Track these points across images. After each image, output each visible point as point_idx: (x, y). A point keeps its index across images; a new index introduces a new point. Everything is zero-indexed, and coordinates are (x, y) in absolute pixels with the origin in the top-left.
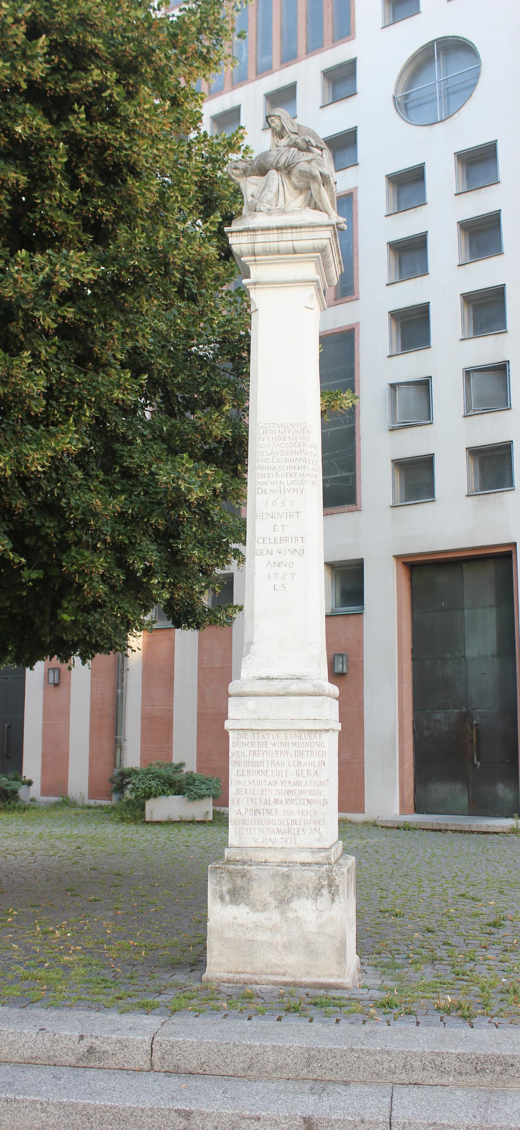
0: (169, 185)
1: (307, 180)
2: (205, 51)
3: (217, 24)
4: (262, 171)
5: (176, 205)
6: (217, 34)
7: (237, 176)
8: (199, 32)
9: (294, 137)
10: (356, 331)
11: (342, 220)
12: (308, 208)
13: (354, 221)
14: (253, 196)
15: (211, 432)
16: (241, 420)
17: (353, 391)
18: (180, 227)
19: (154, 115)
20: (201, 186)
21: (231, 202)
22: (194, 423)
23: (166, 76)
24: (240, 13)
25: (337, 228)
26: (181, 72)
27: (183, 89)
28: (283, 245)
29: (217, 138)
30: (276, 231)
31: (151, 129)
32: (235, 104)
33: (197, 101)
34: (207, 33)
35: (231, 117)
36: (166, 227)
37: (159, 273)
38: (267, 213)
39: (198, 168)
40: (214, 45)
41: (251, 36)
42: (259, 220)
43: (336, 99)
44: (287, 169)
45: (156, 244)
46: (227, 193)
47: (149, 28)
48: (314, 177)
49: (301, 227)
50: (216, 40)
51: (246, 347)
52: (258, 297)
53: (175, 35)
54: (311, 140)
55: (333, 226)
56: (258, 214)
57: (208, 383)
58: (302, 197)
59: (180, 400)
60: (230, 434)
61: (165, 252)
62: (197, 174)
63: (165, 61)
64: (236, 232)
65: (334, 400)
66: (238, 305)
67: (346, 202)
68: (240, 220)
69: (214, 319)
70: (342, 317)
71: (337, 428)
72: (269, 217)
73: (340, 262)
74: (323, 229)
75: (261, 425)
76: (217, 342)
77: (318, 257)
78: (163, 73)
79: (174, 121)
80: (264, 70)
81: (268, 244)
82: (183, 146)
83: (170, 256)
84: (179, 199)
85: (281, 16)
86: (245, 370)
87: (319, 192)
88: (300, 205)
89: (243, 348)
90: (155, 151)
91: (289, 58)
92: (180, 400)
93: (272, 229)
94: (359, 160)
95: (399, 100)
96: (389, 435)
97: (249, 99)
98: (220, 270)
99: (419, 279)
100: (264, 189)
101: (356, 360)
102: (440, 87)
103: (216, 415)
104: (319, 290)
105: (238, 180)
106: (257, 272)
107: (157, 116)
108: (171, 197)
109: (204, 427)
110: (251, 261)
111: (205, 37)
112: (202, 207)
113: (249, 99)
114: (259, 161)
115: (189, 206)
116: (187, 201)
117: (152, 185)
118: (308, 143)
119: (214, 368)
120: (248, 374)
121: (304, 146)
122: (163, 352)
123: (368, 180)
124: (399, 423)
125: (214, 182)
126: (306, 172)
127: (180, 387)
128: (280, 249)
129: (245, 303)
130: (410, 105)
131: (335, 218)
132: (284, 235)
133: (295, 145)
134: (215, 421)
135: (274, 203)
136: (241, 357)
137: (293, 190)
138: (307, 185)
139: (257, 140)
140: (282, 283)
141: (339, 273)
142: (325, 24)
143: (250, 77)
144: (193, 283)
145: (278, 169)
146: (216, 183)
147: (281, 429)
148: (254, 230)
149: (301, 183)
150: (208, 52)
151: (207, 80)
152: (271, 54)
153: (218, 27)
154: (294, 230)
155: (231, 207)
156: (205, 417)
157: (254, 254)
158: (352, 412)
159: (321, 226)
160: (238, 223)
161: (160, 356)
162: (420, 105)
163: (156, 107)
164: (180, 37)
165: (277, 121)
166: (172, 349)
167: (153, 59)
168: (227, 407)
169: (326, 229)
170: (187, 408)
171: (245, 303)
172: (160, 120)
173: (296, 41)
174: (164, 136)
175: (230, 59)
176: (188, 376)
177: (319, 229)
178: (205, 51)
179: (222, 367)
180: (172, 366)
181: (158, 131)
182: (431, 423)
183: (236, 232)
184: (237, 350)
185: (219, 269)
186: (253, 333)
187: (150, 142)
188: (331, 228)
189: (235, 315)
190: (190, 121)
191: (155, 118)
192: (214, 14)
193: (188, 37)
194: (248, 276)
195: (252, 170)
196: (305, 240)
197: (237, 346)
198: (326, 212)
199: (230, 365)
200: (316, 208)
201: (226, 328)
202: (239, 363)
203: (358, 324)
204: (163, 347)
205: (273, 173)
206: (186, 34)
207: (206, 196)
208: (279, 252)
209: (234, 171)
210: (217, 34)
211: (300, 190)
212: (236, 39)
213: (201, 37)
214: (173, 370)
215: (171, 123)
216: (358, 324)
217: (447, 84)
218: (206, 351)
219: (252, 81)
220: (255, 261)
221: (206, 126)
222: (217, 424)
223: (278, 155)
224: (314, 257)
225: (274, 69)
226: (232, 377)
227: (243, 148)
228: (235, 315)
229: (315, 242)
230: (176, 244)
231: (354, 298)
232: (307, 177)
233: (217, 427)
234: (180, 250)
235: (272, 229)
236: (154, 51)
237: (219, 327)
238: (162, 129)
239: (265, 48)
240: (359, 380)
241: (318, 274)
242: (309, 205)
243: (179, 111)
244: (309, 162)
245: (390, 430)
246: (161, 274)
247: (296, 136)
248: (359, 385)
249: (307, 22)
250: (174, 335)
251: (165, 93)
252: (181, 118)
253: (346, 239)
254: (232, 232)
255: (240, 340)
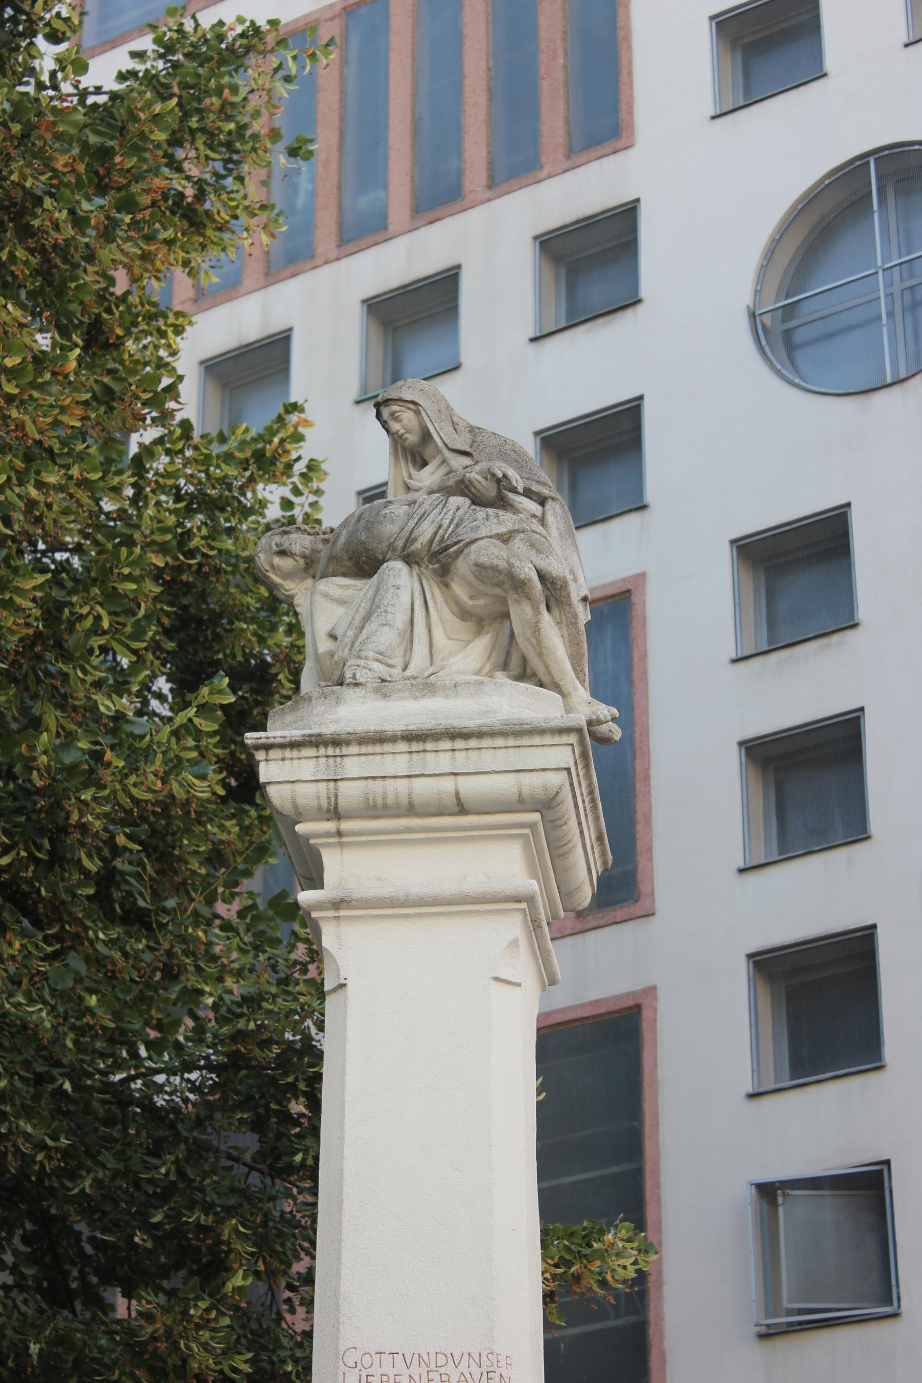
0: (76, 580)
1: (498, 591)
2: (190, 192)
3: (229, 118)
4: (363, 563)
5: (97, 642)
6: (229, 145)
7: (286, 576)
8: (175, 141)
9: (459, 462)
10: (646, 1014)
11: (604, 711)
12: (501, 677)
13: (636, 675)
14: (333, 637)
15: (184, 1361)
16: (280, 1318)
17: (640, 1225)
18: (106, 705)
19: (33, 385)
20: (172, 584)
21: (261, 626)
22: (131, 1332)
23: (76, 266)
24: (292, 87)
25: (592, 738)
26: (119, 256)
27: (123, 298)
28: (424, 788)
29: (223, 439)
30: (402, 746)
31: (21, 426)
32: (276, 326)
33: (162, 334)
34: (200, 144)
35: (262, 363)
36: (62, 707)
37: (32, 857)
38: (377, 691)
39: (165, 530)
40: (219, 177)
41: (324, 143)
42: (353, 712)
43: (576, 318)
44: (438, 560)
45: (30, 769)
46: (248, 599)
47: (25, 136)
48: (519, 586)
49: (479, 734)
50: (226, 162)
51: (302, 1086)
52: (347, 947)
53: (105, 153)
54: (512, 474)
55: (579, 731)
56: (349, 693)
57: (178, 1199)
58: (483, 642)
59: (89, 1249)
60: (247, 1368)
61: (55, 796)
62: (163, 548)
63: (69, 231)
64: (282, 746)
65: (581, 1256)
66: (280, 951)
67: (615, 615)
68: (293, 709)
69: (201, 993)
70: (601, 970)
71: (588, 1328)
72: (382, 703)
73: (600, 838)
74: (548, 740)
75: (351, 1359)
76: (210, 1067)
77: (532, 826)
78: (65, 260)
79: (95, 397)
80: (362, 231)
81: (378, 785)
82: (119, 472)
83: (70, 804)
84: (106, 625)
85: (414, 80)
86: (298, 1158)
87: (536, 630)
88: (476, 665)
89: (293, 1087)
90: (34, 493)
91: (438, 197)
92: (89, 1249)
93: (393, 739)
94: (650, 495)
95: (767, 319)
96: (759, 1349)
97: (320, 315)
98: (227, 831)
99: (841, 854)
100: (367, 618)
101: (647, 1107)
102: (889, 284)
103: (203, 1305)
104: (535, 925)
105: (290, 587)
106: (342, 869)
107: (42, 387)
108: (82, 617)
109: (162, 1346)
110: (328, 834)
111: (193, 154)
112: (170, 645)
113: (320, 315)
114: (352, 534)
115: (136, 645)
116: (129, 629)
117: (19, 591)
118: (502, 482)
119: (198, 1151)
120: (312, 1172)
121: (489, 490)
122: (37, 1097)
123: (676, 554)
124: (790, 1312)
125: (208, 571)
126: (495, 569)
127: (88, 1207)
128: (417, 800)
129: (301, 948)
130: (800, 336)
131: (585, 706)
132: (430, 757)
133: (463, 488)
134: (199, 1327)
135: (398, 661)
136: (288, 1118)
137: (456, 622)
138: (498, 607)
139: (346, 451)
140: (422, 902)
141: (597, 869)
142: (545, 105)
143: (320, 250)
144: (138, 877)
145: (410, 559)
146: (218, 571)
147: (415, 1370)
148: (336, 742)
149: (481, 602)
150: (201, 195)
151: (193, 273)
152: (385, 186)
153: (232, 126)
154: (459, 744)
155: (262, 641)
156: (166, 1310)
157: (335, 813)
158: (639, 1292)
159: (542, 732)
160: (289, 718)
161: (27, 1112)
162: (829, 336)
163: (39, 359)
164: (118, 159)
165: (408, 417)
166: (67, 1086)
167: (36, 223)
168: (238, 1280)
169: (557, 740)
170: (108, 1279)
171: (301, 948)
172: (51, 400)
173: (459, 152)
174: (64, 443)
175: (263, 216)
176: (116, 1174)
177: (537, 740)
178: (190, 192)
179: (223, 1147)
180: (64, 1141)
181: (41, 432)
182: (895, 1315)
183: (282, 746)
184: (274, 1095)
185: (222, 827)
186: (327, 1043)
187: (19, 464)
188: (573, 739)
189: (268, 982)
190: (146, 396)
191: (36, 394)
192: (219, 92)
193: (142, 160)
194: (315, 881)
195: (332, 558)
196: (492, 773)
197: (274, 1080)
198: (556, 687)
199: (249, 1142)
200: (525, 674)
201: (241, 1024)
202: (279, 1136)
203: (651, 991)
204: (40, 1079)
205: (396, 573)
206: (136, 150)
207: (185, 608)
208: (411, 809)
209: (277, 561)
210: (229, 145)
211: (476, 621)
212: (282, 159)
213: (180, 154)
214: (66, 1154)
215: (86, 403)
216: (651, 991)
217: (912, 275)
218: (174, 1088)
219: (327, 262)
220: (339, 834)
221: (190, 404)
222: (205, 1335)
223: (410, 516)
224: (522, 826)
225: (393, 228)
226: (255, 1179)
227: (299, 467)
228: (268, 982)
229: (525, 778)
230: (92, 771)
231: (637, 909)
232: (500, 585)
233: (205, 1346)
234: (101, 786)
235: (393, 739)
236: (39, 201)
237: (222, 1020)
238: (56, 423)
239: (367, 166)
240: (656, 1171)
241: (533, 875)
242: (505, 666)
243: (111, 365)
244: (505, 538)
245: (762, 1336)
246: (37, 861)
247: (467, 461)
248: (657, 1186)
249: (490, 100)
250: (76, 1042)
251: (69, 315)
252: (116, 387)
253: (615, 770)
254: (268, 747)
255: (283, 1063)
